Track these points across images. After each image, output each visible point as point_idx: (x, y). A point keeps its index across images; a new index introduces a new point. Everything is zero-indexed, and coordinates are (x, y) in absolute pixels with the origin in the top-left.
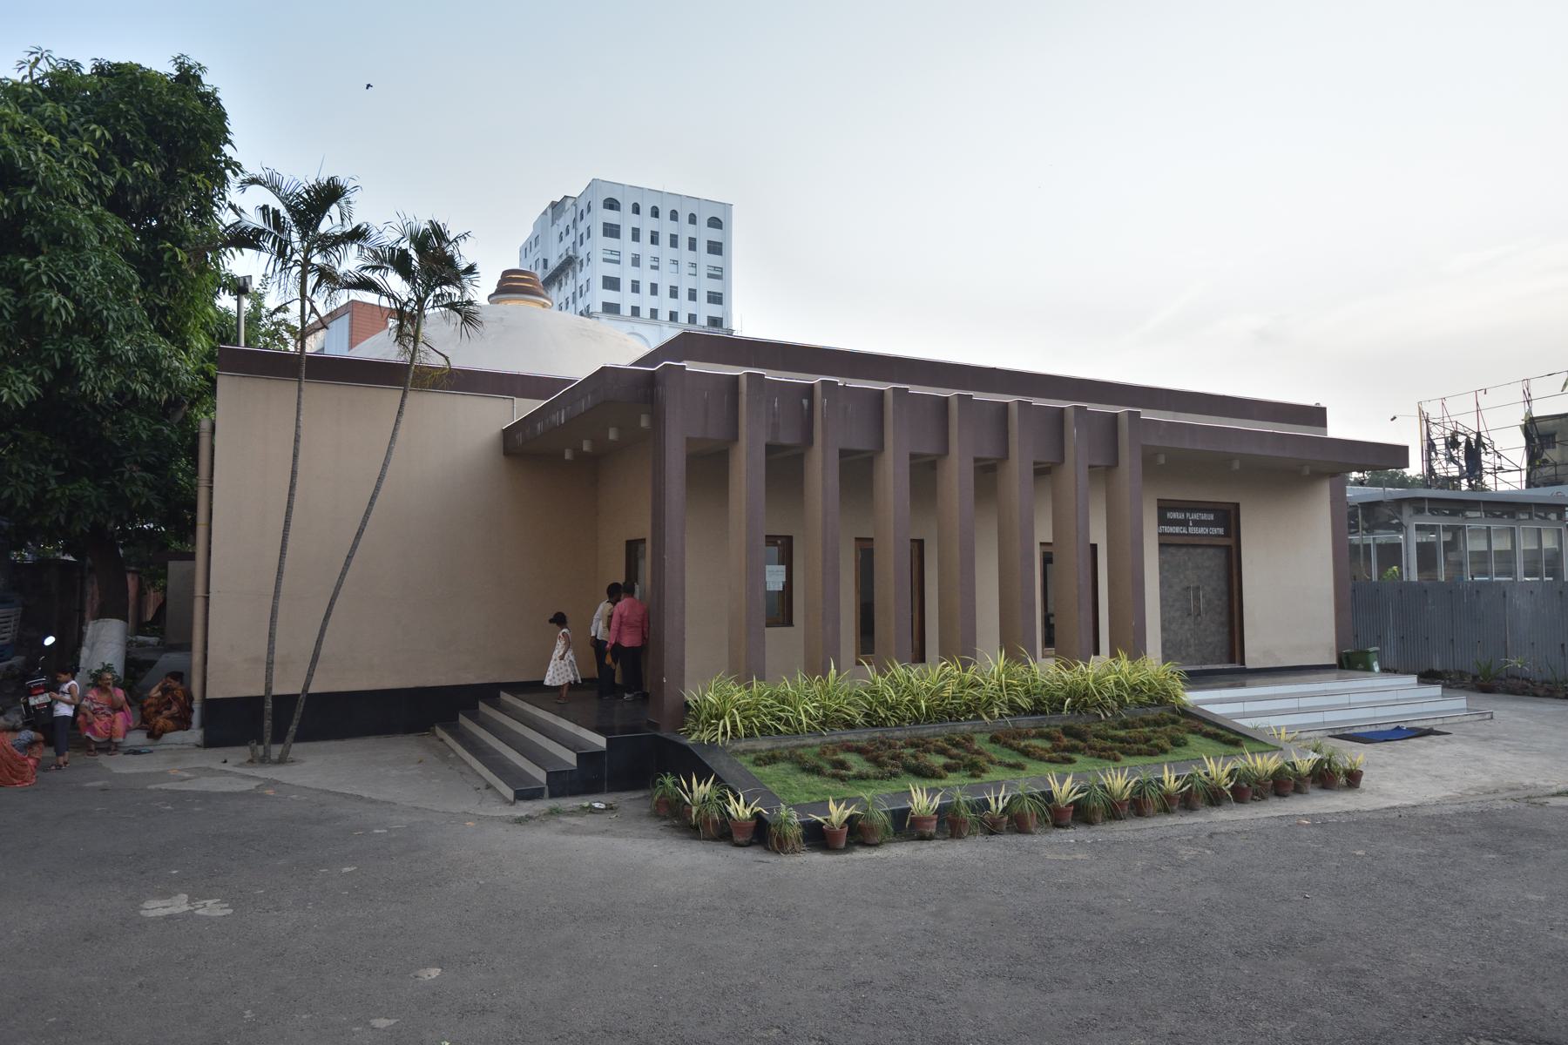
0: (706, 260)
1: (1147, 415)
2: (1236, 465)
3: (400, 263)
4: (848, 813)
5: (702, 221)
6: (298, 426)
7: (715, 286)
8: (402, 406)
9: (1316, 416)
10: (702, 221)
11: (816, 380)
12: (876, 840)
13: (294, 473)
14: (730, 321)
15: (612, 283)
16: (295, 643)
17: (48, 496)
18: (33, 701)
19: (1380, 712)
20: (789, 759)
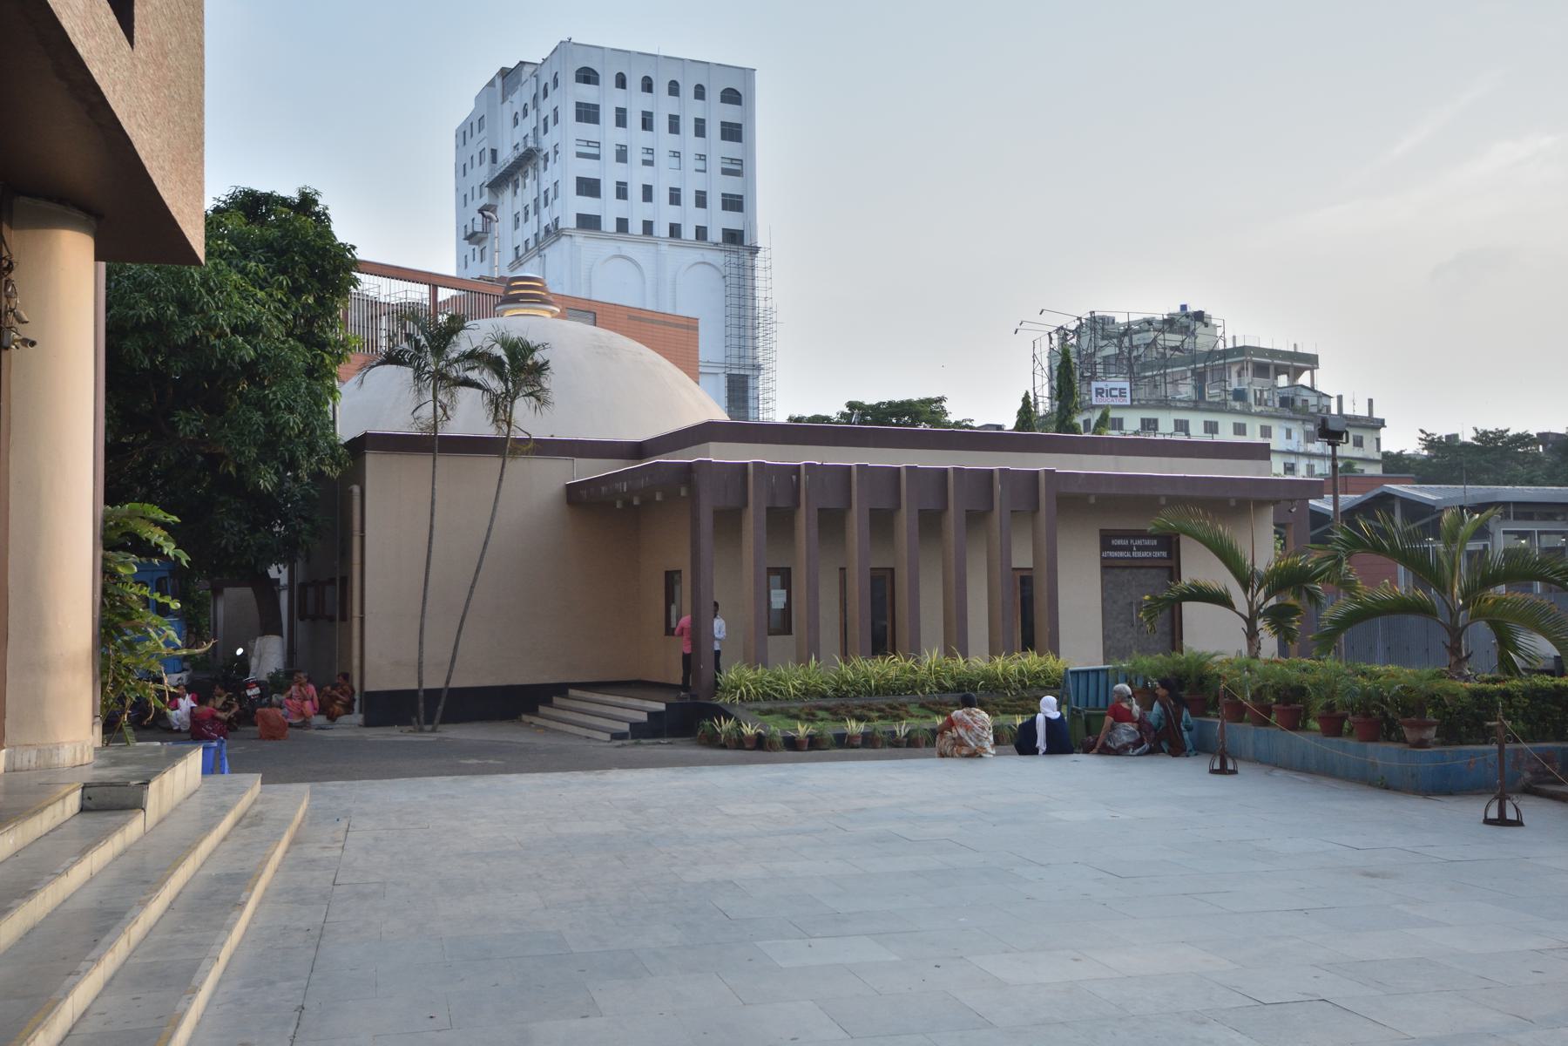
3: (495, 364)
5: (714, 94)
7: (732, 186)
10: (714, 94)
13: (432, 527)
14: (753, 236)
15: (588, 187)
16: (438, 650)
18: (249, 693)
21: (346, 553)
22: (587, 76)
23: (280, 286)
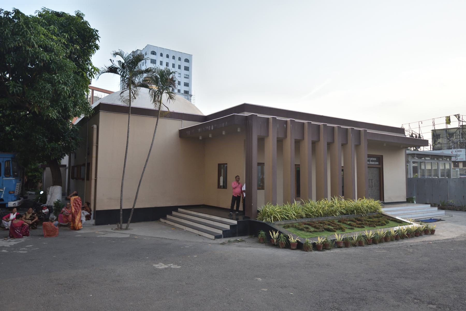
0: (183, 72)
1: (369, 131)
2: (385, 145)
4: (323, 240)
5: (183, 60)
6: (128, 128)
7: (186, 81)
8: (157, 123)
9: (402, 131)
10: (183, 60)
11: (288, 119)
12: (329, 248)
16: (129, 193)
17: (46, 147)
18: (44, 211)
19: (425, 215)
20: (293, 226)
21: (89, 154)
22: (154, 53)
23: (65, 37)
